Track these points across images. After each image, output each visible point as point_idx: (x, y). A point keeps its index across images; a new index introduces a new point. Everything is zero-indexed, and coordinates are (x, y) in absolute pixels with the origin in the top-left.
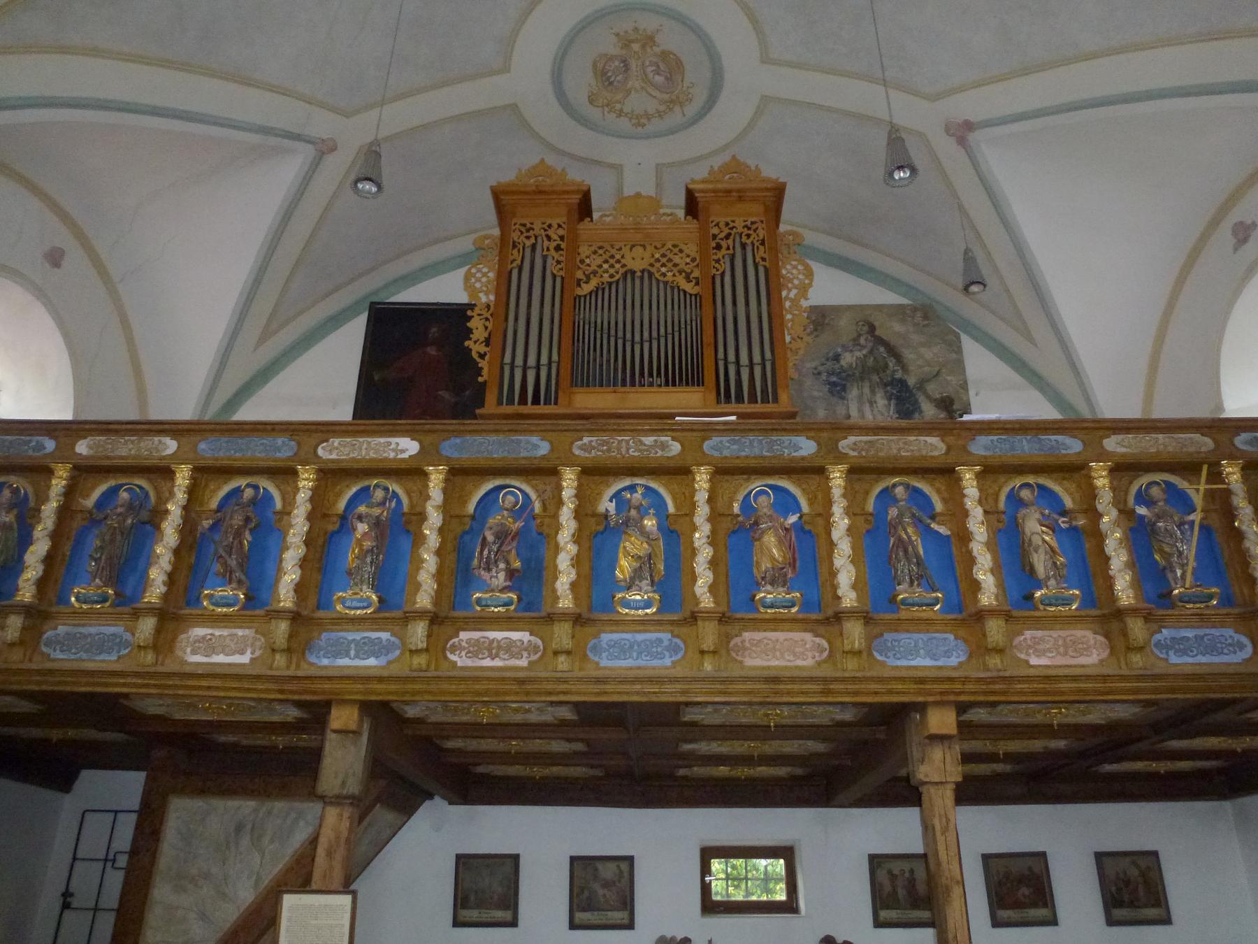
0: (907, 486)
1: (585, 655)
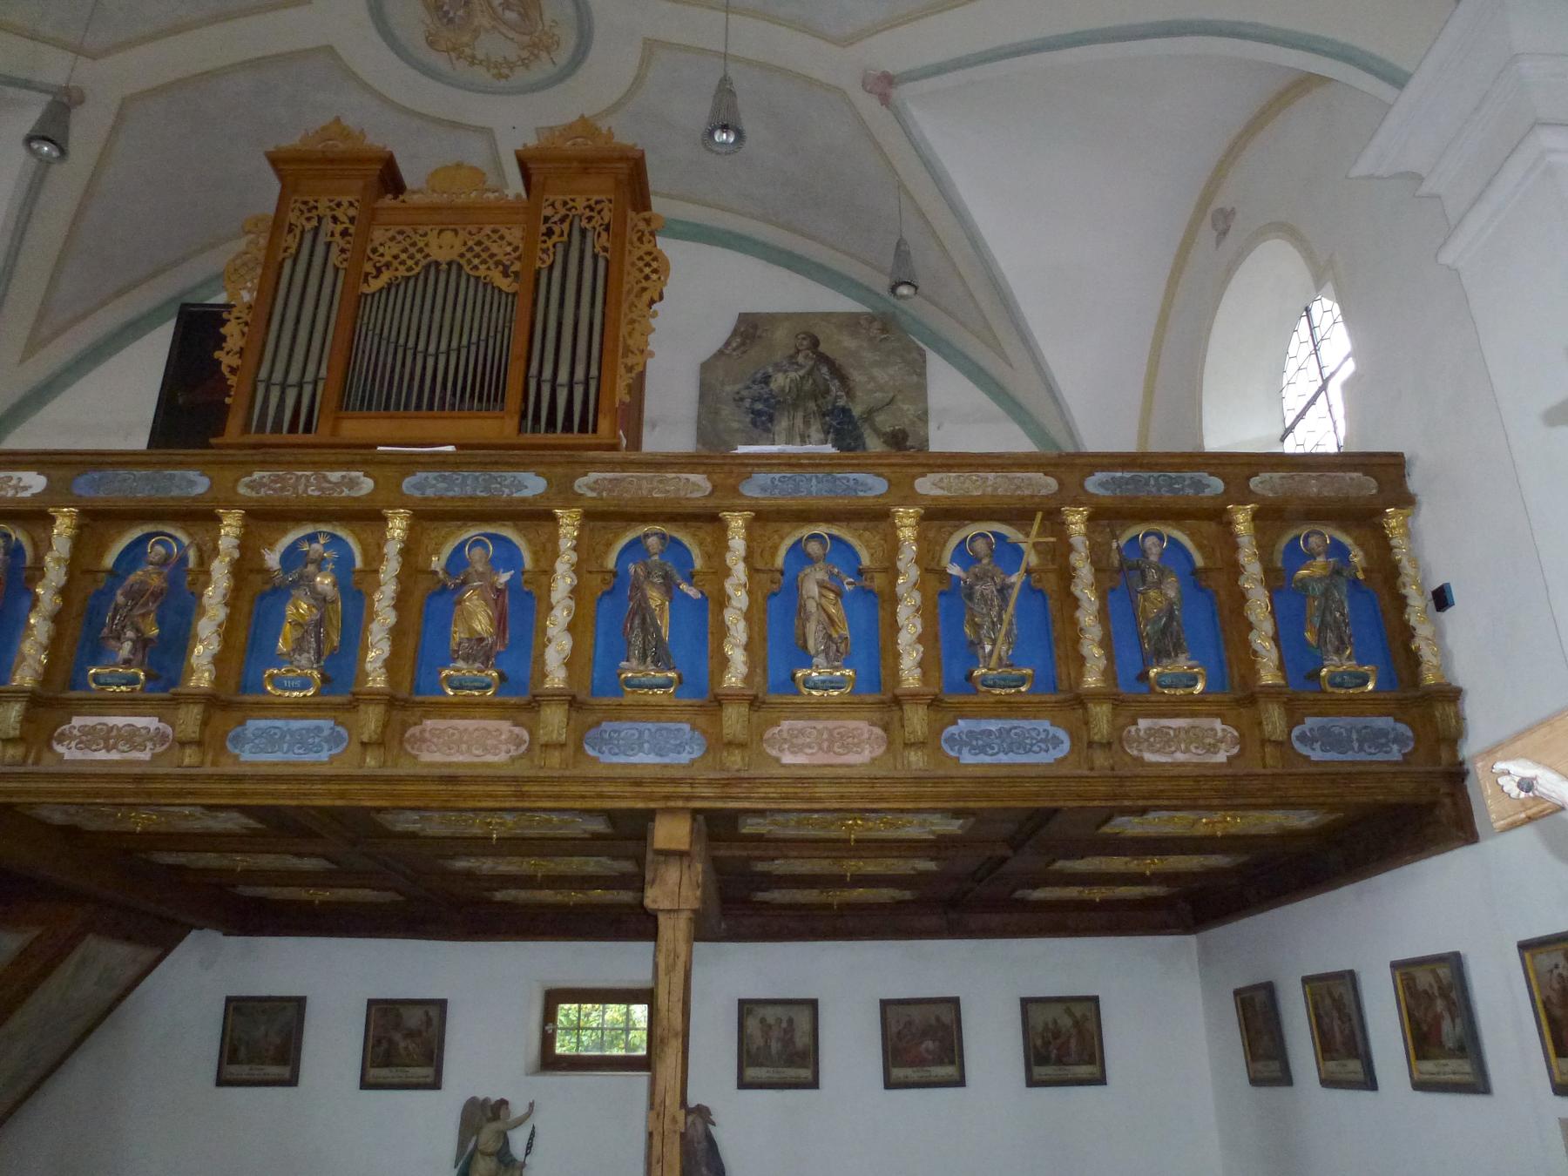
0: (663, 537)
1: (223, 747)
